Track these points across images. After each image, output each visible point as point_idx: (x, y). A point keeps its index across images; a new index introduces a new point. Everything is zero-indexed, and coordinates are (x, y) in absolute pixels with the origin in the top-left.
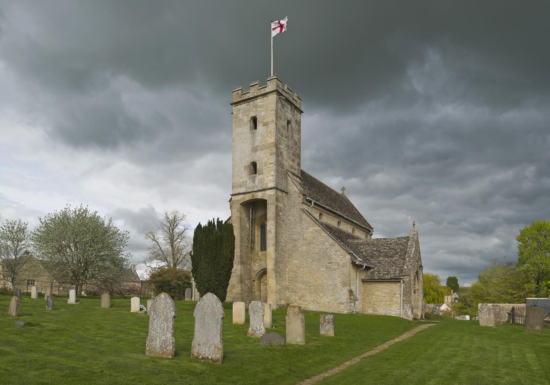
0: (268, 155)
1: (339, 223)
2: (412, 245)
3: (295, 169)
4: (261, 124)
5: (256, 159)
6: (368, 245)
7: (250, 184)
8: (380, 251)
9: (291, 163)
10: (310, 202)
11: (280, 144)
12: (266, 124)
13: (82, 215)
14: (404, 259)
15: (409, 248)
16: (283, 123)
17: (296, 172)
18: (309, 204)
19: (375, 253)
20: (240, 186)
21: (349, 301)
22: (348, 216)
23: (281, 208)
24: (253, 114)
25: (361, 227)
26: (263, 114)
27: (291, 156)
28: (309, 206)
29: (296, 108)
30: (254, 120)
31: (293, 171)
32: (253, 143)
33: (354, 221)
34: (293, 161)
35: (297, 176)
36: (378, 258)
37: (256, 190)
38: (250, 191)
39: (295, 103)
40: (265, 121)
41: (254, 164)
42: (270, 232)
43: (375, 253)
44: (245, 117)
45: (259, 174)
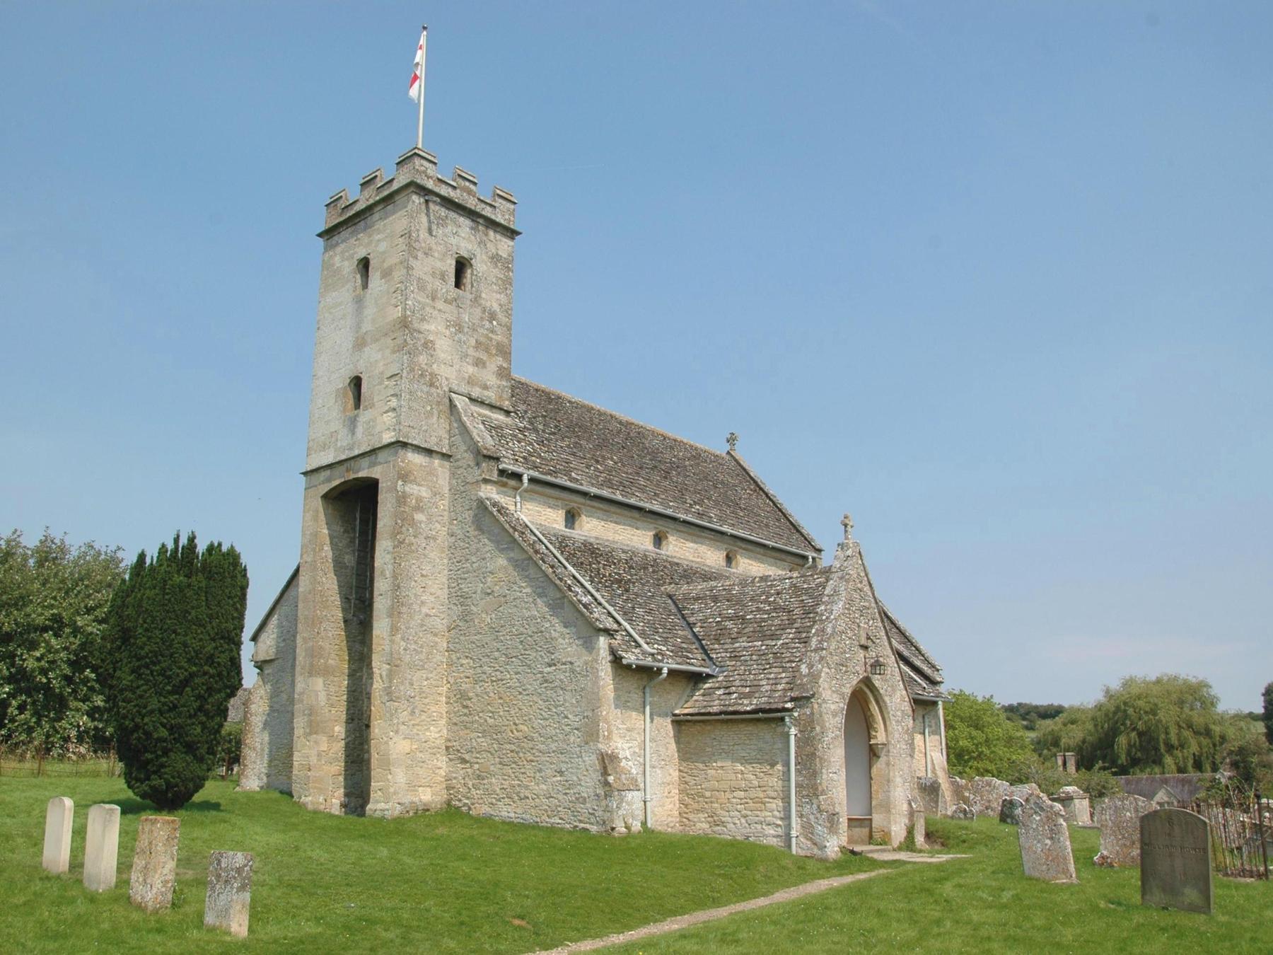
0: (388, 352)
1: (658, 540)
2: (836, 592)
3: (486, 387)
4: (378, 273)
5: (361, 368)
6: (715, 599)
7: (344, 439)
8: (743, 618)
9: (471, 369)
10: (518, 476)
11: (423, 320)
12: (387, 274)
13: (1204, 685)
14: (806, 642)
15: (826, 603)
16: (438, 264)
17: (490, 395)
18: (512, 483)
19: (729, 624)
20: (324, 447)
21: (600, 791)
22: (700, 515)
23: (419, 499)
24: (362, 253)
25: (764, 546)
26: (383, 247)
27: (471, 352)
28: (516, 489)
29: (492, 224)
30: (365, 264)
31: (476, 392)
32: (358, 327)
33: (725, 529)
34: (479, 363)
35: (492, 407)
36: (734, 640)
37: (356, 452)
38: (343, 457)
39: (487, 212)
40: (386, 265)
41: (357, 382)
42: (382, 573)
43: (729, 624)
44: (346, 263)
45: (366, 408)
